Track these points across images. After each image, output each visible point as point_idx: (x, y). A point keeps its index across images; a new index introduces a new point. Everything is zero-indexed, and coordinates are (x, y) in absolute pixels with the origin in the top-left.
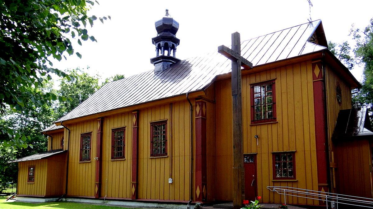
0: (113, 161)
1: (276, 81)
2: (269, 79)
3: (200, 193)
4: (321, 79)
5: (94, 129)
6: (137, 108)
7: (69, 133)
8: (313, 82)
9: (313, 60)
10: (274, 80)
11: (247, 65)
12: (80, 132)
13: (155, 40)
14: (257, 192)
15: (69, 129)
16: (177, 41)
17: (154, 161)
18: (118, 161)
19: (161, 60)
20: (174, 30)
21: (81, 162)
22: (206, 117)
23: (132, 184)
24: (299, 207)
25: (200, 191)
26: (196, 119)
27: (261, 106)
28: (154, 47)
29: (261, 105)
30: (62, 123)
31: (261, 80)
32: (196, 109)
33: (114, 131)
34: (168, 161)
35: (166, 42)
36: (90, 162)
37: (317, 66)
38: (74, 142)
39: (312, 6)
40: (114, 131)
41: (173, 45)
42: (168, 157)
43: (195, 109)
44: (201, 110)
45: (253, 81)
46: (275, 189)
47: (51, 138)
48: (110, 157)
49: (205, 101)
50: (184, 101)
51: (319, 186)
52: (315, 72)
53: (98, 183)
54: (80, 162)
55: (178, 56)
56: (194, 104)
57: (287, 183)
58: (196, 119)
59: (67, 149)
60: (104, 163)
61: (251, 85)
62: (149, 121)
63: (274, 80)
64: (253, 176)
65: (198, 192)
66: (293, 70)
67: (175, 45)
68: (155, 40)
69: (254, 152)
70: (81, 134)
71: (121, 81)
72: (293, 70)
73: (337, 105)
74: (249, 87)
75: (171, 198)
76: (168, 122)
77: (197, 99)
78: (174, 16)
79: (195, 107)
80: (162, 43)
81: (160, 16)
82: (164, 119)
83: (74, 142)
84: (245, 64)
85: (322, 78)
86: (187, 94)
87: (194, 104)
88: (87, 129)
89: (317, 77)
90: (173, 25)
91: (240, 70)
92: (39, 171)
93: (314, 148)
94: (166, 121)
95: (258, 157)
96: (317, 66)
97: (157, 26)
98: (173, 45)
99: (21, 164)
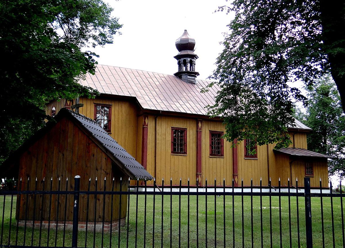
13: (177, 57)
16: (194, 57)
28: (176, 61)
68: (177, 57)
78: (192, 36)
81: (177, 37)
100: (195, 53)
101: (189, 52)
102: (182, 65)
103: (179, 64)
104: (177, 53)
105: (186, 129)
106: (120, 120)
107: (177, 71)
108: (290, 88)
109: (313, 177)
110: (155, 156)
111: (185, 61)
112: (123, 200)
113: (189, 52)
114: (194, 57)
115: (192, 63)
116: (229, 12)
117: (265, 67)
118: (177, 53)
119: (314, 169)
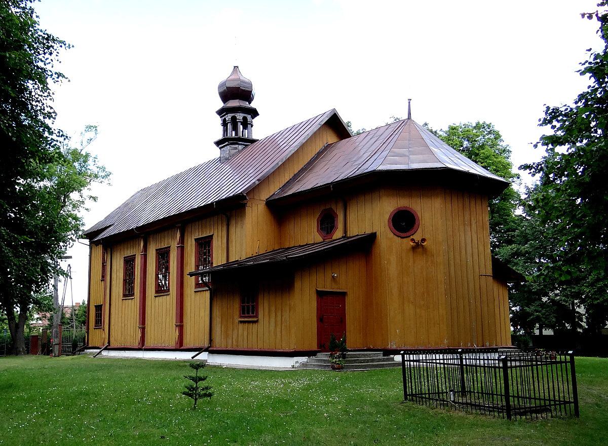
13: (220, 112)
14: (199, 208)
16: (254, 113)
19: (227, 143)
20: (247, 95)
21: (125, 298)
23: (176, 326)
28: (218, 120)
35: (233, 114)
41: (245, 119)
54: (123, 298)
55: (254, 137)
67: (249, 117)
68: (220, 112)
71: (205, 203)
75: (234, 346)
78: (248, 75)
80: (229, 117)
81: (223, 75)
90: (241, 78)
92: (266, 305)
97: (222, 90)
98: (245, 119)
100: (253, 105)
101: (245, 104)
102: (229, 126)
103: (225, 124)
104: (220, 104)
105: (344, 294)
106: (450, 229)
107: (219, 136)
108: (26, 5)
109: (256, 322)
110: (91, 261)
111: (234, 119)
112: (99, 286)
113: (245, 104)
114: (254, 113)
115: (246, 124)
116: (590, 17)
117: (26, 95)
118: (220, 104)
119: (260, 301)
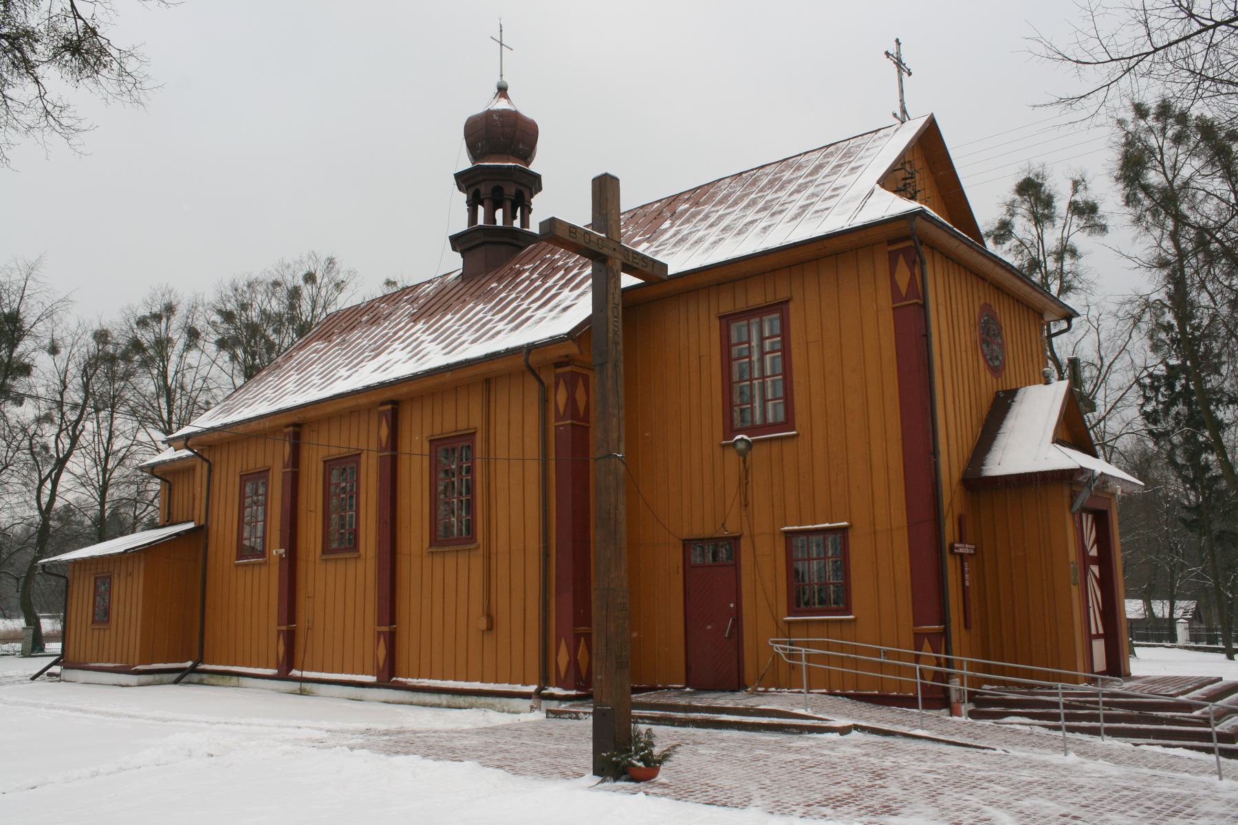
0: (326, 560)
1: (792, 306)
2: (770, 299)
3: (569, 663)
4: (915, 301)
5: (276, 456)
6: (389, 394)
7: (210, 471)
8: (894, 309)
9: (891, 242)
10: (787, 302)
11: (646, 269)
12: (427, 432)
13: (463, 180)
15: (208, 461)
17: (438, 560)
18: (340, 559)
22: (589, 423)
24: (477, 696)
25: (570, 657)
26: (556, 427)
27: (751, 386)
29: (751, 380)
30: (187, 441)
31: (749, 304)
32: (555, 395)
33: (329, 464)
34: (477, 562)
36: (265, 563)
37: (901, 261)
38: (222, 502)
39: (910, 74)
40: (329, 464)
42: (478, 547)
43: (553, 392)
44: (572, 400)
45: (726, 307)
46: (772, 642)
47: (167, 485)
48: (426, 544)
49: (585, 372)
50: (369, 409)
51: (915, 634)
52: (897, 277)
53: (385, 629)
56: (549, 378)
57: (827, 625)
58: (556, 427)
59: (203, 522)
60: (301, 567)
61: (721, 318)
62: (425, 436)
63: (787, 302)
64: (732, 605)
65: (563, 658)
66: (775, 285)
68: (463, 180)
69: (732, 528)
70: (241, 476)
72: (775, 285)
73: (986, 376)
74: (716, 324)
76: (478, 436)
77: (558, 365)
79: (553, 389)
80: (485, 189)
82: (442, 434)
83: (222, 502)
84: (638, 269)
85: (919, 298)
86: (524, 351)
87: (549, 378)
88: (256, 458)
89: (904, 295)
91: (618, 292)
93: (900, 518)
94: (474, 434)
95: (745, 544)
96: (901, 261)
99: (77, 567)
